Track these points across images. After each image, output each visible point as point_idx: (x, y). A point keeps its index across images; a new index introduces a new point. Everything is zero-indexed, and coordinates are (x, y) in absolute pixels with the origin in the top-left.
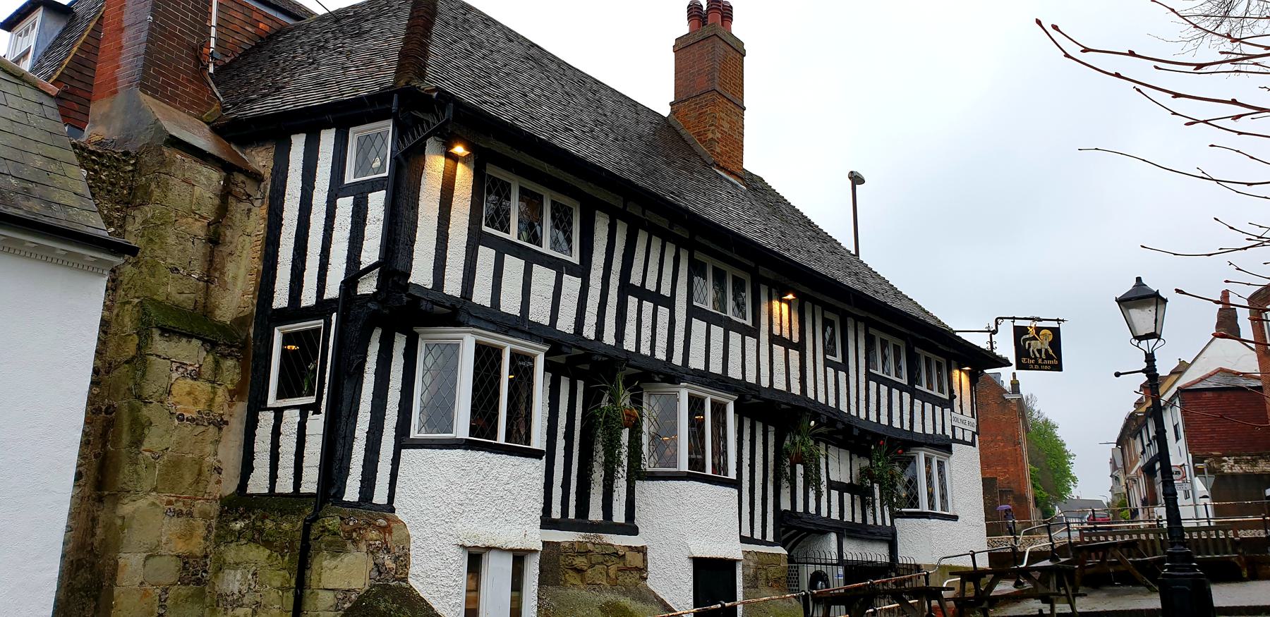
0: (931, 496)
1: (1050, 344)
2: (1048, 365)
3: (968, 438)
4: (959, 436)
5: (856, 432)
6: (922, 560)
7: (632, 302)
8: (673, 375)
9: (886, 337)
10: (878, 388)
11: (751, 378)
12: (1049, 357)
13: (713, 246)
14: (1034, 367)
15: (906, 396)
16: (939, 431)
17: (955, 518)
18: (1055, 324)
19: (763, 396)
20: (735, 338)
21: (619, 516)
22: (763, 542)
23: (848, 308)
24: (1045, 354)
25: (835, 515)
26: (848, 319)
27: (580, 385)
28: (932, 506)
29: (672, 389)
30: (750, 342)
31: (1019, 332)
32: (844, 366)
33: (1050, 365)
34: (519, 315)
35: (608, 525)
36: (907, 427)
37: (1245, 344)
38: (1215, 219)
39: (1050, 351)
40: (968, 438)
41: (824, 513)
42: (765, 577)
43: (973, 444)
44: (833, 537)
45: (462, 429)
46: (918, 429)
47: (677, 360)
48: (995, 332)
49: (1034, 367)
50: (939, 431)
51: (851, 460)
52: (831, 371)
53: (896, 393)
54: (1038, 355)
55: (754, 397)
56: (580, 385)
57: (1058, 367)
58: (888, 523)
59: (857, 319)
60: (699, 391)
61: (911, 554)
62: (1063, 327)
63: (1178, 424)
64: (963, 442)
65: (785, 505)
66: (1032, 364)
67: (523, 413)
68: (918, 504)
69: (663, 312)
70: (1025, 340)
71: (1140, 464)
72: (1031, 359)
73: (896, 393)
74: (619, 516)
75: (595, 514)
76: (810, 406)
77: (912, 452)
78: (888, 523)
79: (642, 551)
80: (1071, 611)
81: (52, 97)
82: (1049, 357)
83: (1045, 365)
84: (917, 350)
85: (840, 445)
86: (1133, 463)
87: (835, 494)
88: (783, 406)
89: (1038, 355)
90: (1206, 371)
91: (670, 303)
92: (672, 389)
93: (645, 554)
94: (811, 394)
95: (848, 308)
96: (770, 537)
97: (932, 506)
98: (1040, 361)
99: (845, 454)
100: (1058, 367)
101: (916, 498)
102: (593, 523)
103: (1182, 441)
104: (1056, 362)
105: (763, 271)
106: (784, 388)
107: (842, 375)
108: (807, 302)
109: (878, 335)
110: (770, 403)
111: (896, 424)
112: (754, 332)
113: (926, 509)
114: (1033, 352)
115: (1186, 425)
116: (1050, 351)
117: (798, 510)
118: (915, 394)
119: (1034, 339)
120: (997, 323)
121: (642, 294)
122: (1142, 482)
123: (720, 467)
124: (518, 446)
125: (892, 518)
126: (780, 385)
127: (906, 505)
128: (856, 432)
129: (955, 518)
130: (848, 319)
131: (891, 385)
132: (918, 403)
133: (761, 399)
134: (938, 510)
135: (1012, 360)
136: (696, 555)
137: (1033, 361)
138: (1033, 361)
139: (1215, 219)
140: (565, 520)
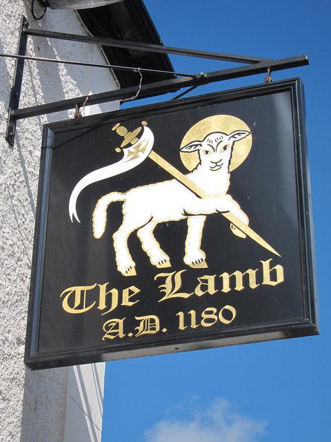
1: (240, 186)
2: (219, 300)
13: (82, 395)
14: (131, 325)
24: (207, 244)
26: (133, 273)
33: (233, 297)
38: (305, 63)
39: (240, 222)
49: (131, 325)
54: (158, 256)
67: (48, 151)
72: (120, 282)
83: (199, 304)
89: (158, 256)
98: (171, 288)
104: (273, 275)
114: (134, 242)
116: (240, 222)
130: (133, 273)
139: (305, 63)
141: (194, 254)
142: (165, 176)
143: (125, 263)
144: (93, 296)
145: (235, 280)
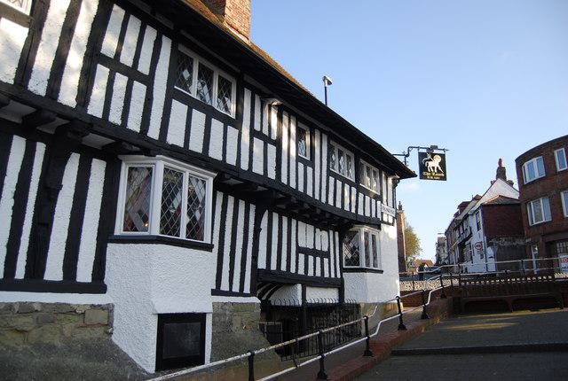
0: (367, 257)
3: (391, 221)
4: (385, 219)
5: (318, 212)
6: (360, 300)
7: (102, 72)
8: (149, 147)
9: (342, 148)
10: (335, 182)
11: (231, 160)
12: (439, 172)
15: (354, 190)
16: (374, 215)
17: (382, 272)
18: (442, 152)
19: (241, 177)
20: (217, 125)
21: (84, 274)
22: (241, 293)
23: (316, 123)
25: (301, 272)
27: (41, 148)
28: (368, 264)
29: (149, 161)
30: (232, 131)
31: (422, 156)
32: (311, 163)
35: (69, 283)
36: (353, 211)
39: (440, 169)
40: (391, 221)
41: (293, 270)
42: (240, 322)
43: (393, 225)
44: (299, 287)
45: (155, 228)
46: (360, 212)
47: (154, 133)
48: (407, 156)
50: (374, 215)
51: (315, 232)
52: (301, 166)
53: (347, 187)
55: (233, 177)
56: (41, 148)
57: (444, 178)
58: (339, 276)
59: (322, 132)
60: (176, 165)
61: (354, 297)
62: (447, 154)
64: (388, 223)
65: (262, 264)
69: (139, 89)
70: (425, 161)
71: (458, 242)
73: (347, 187)
74: (84, 274)
75: (54, 270)
76: (284, 190)
77: (356, 228)
78: (339, 276)
79: (109, 309)
80: (119, 122)
82: (439, 172)
84: (362, 161)
85: (306, 221)
86: (453, 243)
87: (302, 256)
88: (260, 188)
91: (149, 81)
92: (149, 161)
93: (112, 311)
94: (284, 180)
95: (316, 123)
96: (247, 290)
97: (368, 264)
99: (311, 228)
100: (444, 178)
101: (358, 259)
103: (481, 231)
104: (443, 175)
105: (248, 79)
106: (194, 111)
107: (309, 169)
109: (337, 147)
110: (248, 183)
111: (347, 208)
112: (236, 123)
113: (364, 266)
115: (484, 222)
116: (440, 169)
117: (259, 267)
118: (360, 190)
119: (430, 160)
120: (409, 151)
121: (114, 64)
122: (457, 250)
123: (195, 228)
124: (194, 240)
125: (343, 270)
126: (258, 169)
127: (353, 265)
128: (318, 212)
129: (382, 272)
131: (344, 181)
132: (361, 195)
133: (241, 180)
134: (372, 267)
135: (417, 173)
136: (159, 312)
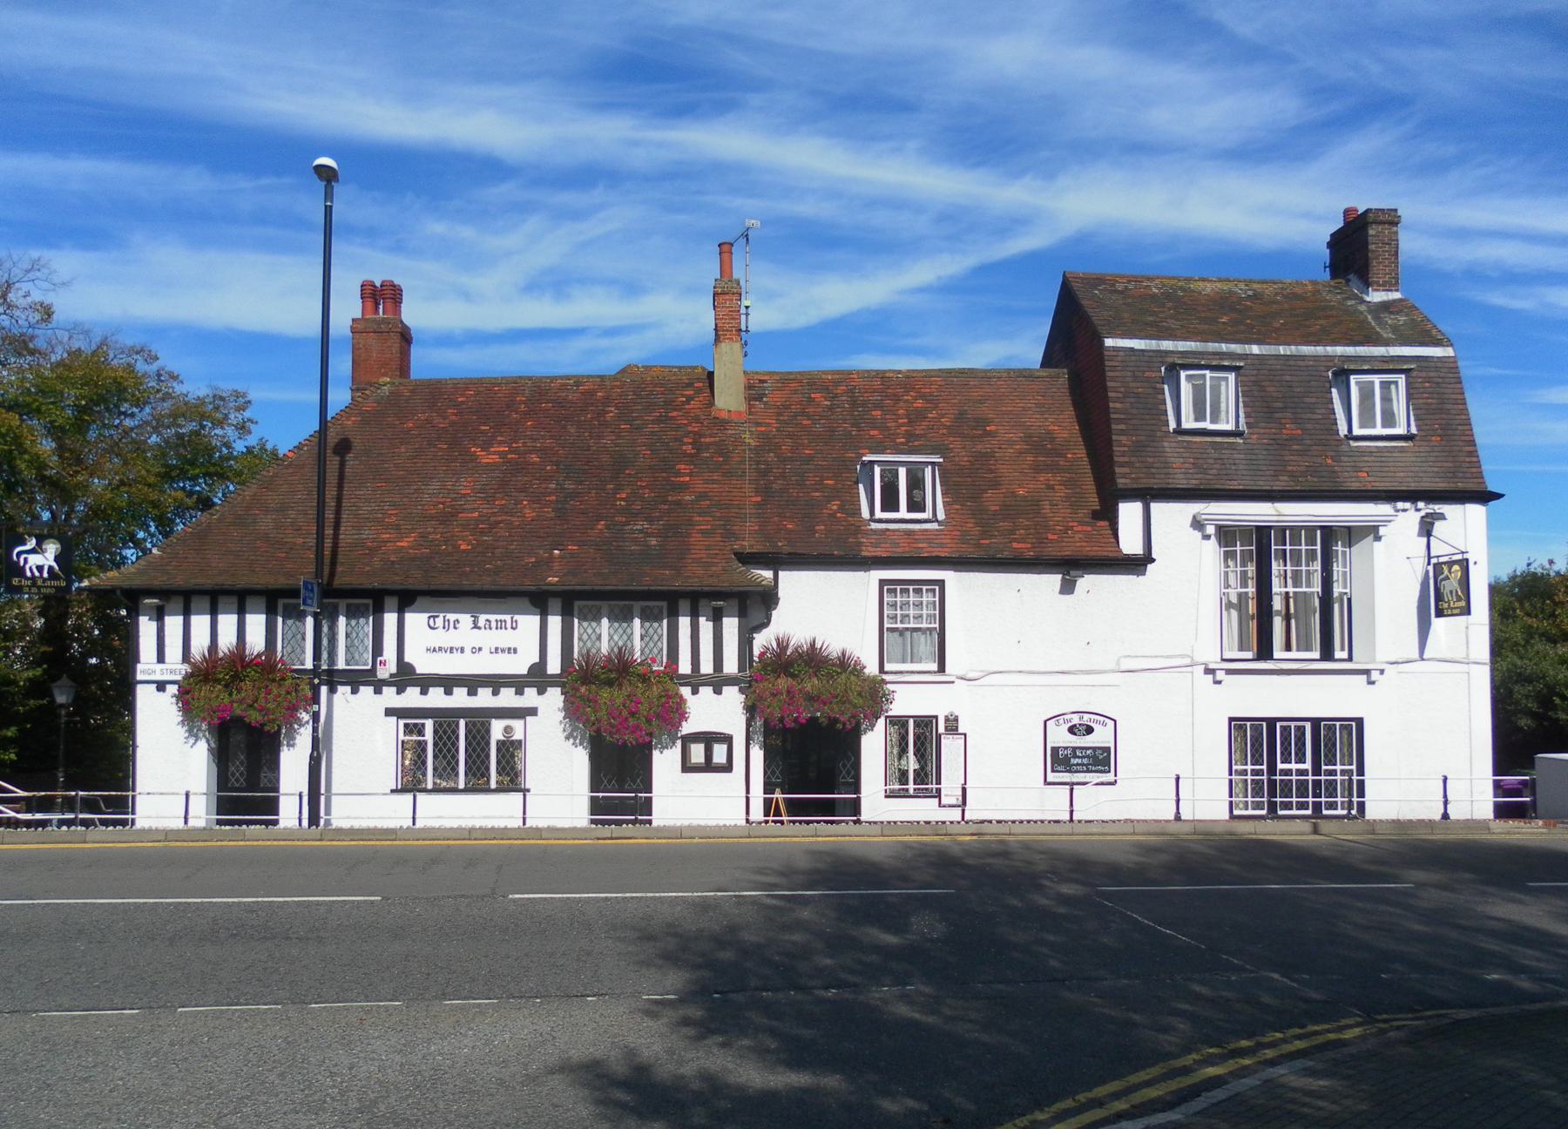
14: (30, 589)
33: (54, 587)
34: (65, 675)
37: (982, 671)
49: (30, 589)
54: (37, 574)
63: (662, 635)
66: (27, 586)
68: (497, 744)
70: (19, 554)
81: (935, 672)
89: (37, 574)
90: (734, 635)
98: (40, 583)
102: (903, 466)
108: (605, 619)
114: (31, 569)
137: (29, 583)
138: (29, 583)
140: (627, 835)
141: (45, 575)
142: (39, 553)
143: (29, 574)
144: (20, 581)
145: (55, 583)
